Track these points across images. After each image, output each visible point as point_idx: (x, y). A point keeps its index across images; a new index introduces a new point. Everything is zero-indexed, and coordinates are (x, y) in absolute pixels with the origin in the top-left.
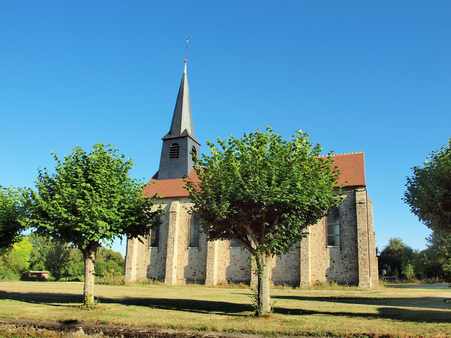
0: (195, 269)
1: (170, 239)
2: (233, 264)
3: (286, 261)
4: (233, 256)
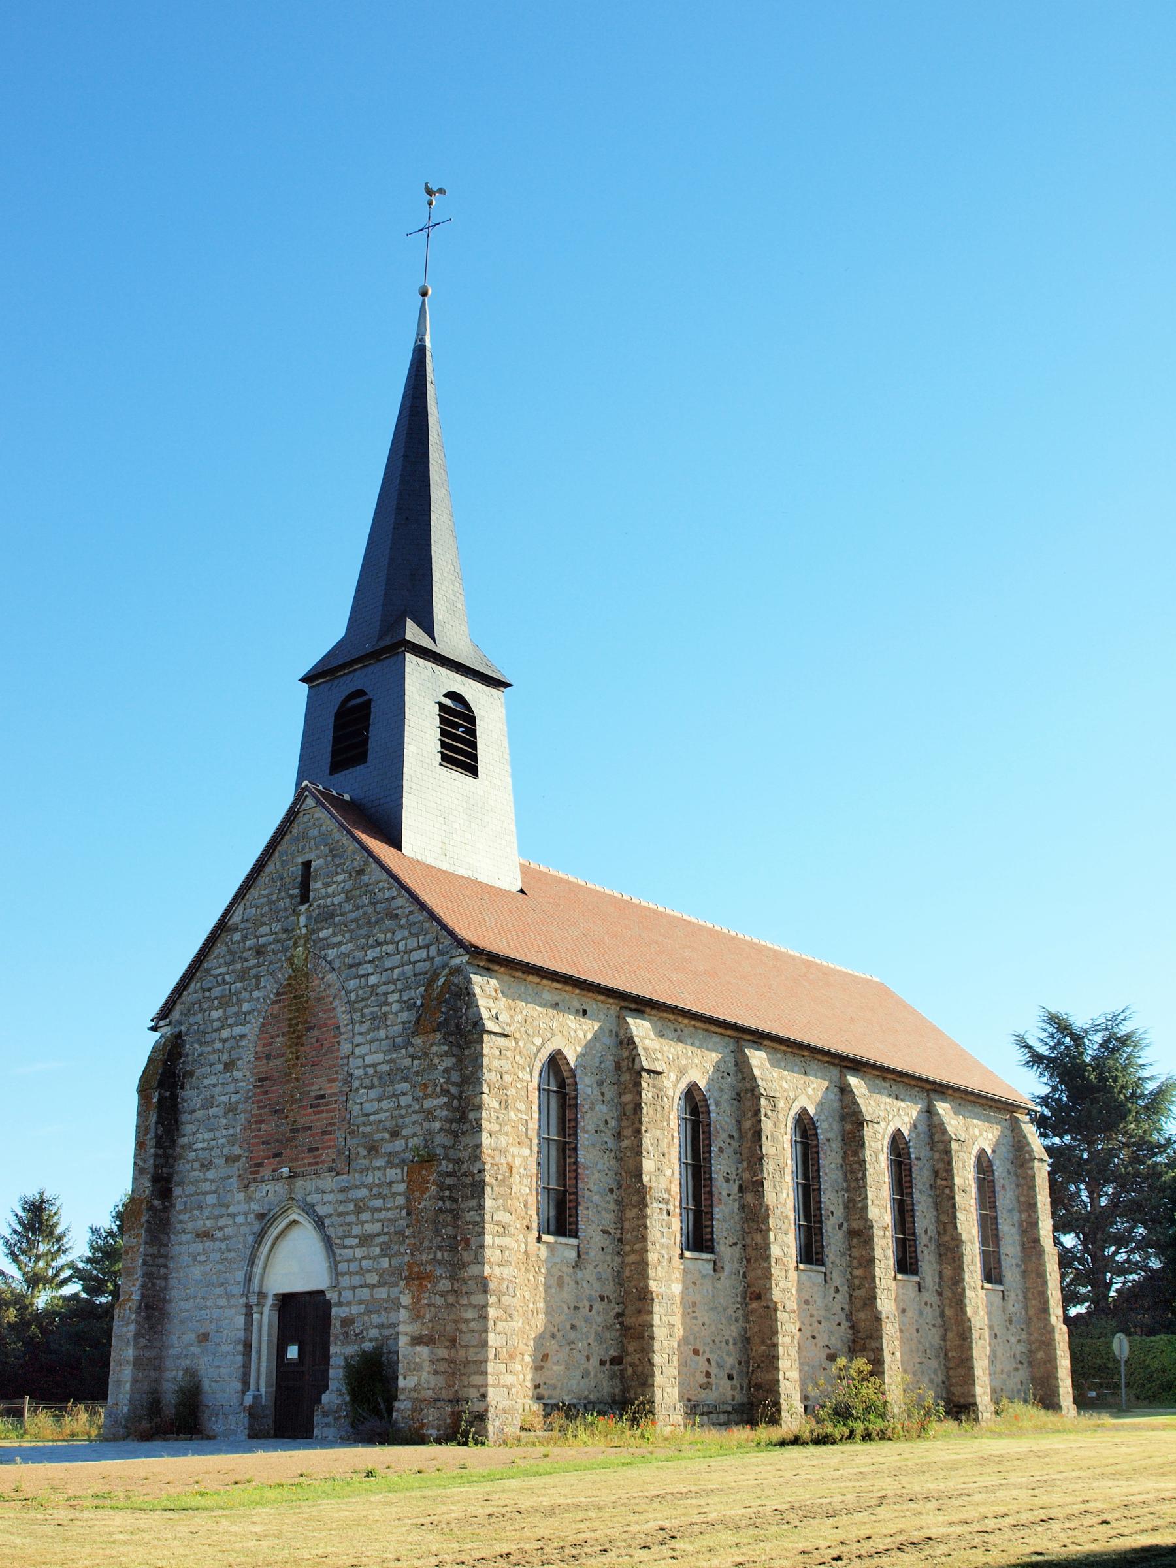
0: (707, 1356)
1: (655, 1205)
2: (809, 1334)
3: (918, 1331)
4: (807, 1302)
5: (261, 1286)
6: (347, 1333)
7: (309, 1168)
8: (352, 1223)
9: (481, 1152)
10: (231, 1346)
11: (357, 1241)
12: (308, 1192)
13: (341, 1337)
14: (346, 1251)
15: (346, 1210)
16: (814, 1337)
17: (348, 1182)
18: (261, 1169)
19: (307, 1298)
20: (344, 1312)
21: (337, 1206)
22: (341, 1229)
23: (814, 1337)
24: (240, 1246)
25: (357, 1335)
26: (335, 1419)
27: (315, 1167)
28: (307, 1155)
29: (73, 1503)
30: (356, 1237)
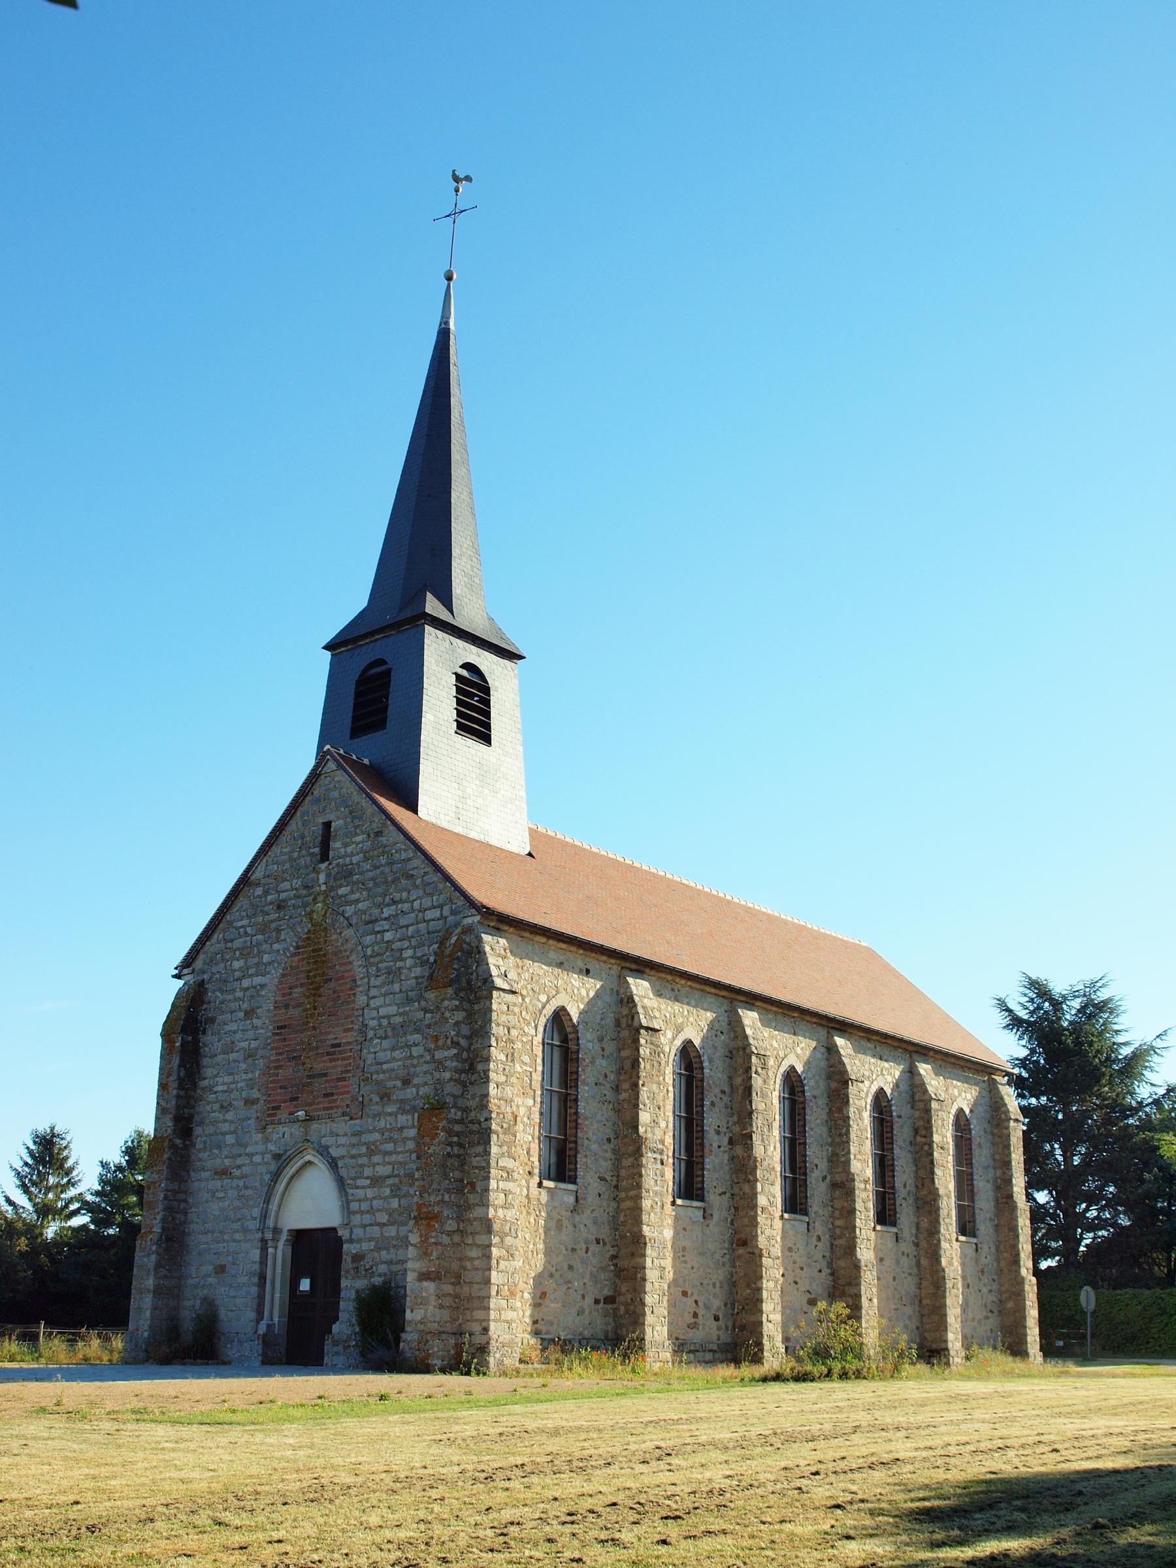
0: (695, 1297)
4: (790, 1249)
13: (352, 1272)
14: (358, 1191)
16: (796, 1283)
17: (361, 1126)
18: (278, 1112)
23: (796, 1283)
26: (345, 1348)
30: (367, 1178)
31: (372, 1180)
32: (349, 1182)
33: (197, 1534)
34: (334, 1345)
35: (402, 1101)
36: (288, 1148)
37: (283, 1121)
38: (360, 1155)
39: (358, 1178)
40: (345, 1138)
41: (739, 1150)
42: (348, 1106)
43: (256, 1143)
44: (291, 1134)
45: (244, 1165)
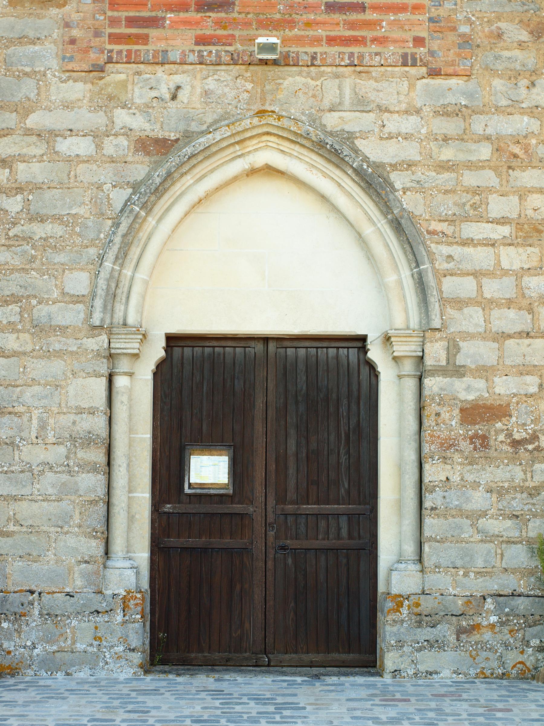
5: (141, 311)
6: (484, 438)
7: (334, 50)
8: (490, 190)
9: (360, 12)
10: (62, 450)
11: (505, 230)
12: (326, 103)
13: (466, 446)
14: (469, 250)
15: (462, 157)
17: (470, 96)
18: (153, 33)
19: (259, 347)
20: (468, 389)
21: (433, 145)
22: (450, 200)
24: (81, 211)
25: (516, 444)
26: (460, 632)
27: (356, 50)
28: (323, 17)
29: (479, 602)
30: (503, 221)
31: (519, 226)
32: (435, 226)
33: (426, 694)
34: (419, 624)
35: (515, 19)
36: (194, 127)
37: (174, 55)
38: (471, 166)
39: (467, 219)
40: (414, 119)
41: (269, 63)
42: (419, 41)
43: (67, 106)
44: (206, 93)
45: (23, 159)
